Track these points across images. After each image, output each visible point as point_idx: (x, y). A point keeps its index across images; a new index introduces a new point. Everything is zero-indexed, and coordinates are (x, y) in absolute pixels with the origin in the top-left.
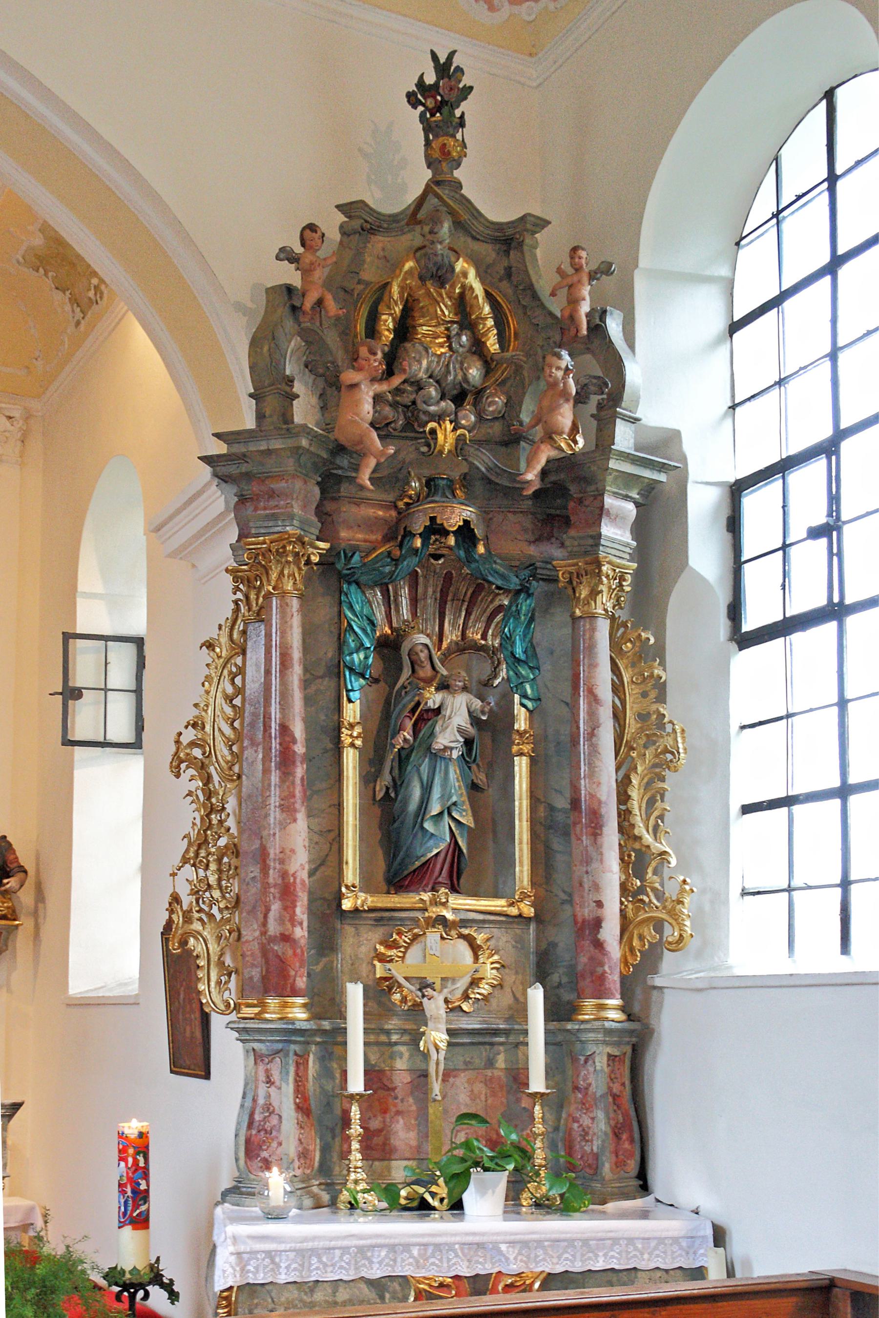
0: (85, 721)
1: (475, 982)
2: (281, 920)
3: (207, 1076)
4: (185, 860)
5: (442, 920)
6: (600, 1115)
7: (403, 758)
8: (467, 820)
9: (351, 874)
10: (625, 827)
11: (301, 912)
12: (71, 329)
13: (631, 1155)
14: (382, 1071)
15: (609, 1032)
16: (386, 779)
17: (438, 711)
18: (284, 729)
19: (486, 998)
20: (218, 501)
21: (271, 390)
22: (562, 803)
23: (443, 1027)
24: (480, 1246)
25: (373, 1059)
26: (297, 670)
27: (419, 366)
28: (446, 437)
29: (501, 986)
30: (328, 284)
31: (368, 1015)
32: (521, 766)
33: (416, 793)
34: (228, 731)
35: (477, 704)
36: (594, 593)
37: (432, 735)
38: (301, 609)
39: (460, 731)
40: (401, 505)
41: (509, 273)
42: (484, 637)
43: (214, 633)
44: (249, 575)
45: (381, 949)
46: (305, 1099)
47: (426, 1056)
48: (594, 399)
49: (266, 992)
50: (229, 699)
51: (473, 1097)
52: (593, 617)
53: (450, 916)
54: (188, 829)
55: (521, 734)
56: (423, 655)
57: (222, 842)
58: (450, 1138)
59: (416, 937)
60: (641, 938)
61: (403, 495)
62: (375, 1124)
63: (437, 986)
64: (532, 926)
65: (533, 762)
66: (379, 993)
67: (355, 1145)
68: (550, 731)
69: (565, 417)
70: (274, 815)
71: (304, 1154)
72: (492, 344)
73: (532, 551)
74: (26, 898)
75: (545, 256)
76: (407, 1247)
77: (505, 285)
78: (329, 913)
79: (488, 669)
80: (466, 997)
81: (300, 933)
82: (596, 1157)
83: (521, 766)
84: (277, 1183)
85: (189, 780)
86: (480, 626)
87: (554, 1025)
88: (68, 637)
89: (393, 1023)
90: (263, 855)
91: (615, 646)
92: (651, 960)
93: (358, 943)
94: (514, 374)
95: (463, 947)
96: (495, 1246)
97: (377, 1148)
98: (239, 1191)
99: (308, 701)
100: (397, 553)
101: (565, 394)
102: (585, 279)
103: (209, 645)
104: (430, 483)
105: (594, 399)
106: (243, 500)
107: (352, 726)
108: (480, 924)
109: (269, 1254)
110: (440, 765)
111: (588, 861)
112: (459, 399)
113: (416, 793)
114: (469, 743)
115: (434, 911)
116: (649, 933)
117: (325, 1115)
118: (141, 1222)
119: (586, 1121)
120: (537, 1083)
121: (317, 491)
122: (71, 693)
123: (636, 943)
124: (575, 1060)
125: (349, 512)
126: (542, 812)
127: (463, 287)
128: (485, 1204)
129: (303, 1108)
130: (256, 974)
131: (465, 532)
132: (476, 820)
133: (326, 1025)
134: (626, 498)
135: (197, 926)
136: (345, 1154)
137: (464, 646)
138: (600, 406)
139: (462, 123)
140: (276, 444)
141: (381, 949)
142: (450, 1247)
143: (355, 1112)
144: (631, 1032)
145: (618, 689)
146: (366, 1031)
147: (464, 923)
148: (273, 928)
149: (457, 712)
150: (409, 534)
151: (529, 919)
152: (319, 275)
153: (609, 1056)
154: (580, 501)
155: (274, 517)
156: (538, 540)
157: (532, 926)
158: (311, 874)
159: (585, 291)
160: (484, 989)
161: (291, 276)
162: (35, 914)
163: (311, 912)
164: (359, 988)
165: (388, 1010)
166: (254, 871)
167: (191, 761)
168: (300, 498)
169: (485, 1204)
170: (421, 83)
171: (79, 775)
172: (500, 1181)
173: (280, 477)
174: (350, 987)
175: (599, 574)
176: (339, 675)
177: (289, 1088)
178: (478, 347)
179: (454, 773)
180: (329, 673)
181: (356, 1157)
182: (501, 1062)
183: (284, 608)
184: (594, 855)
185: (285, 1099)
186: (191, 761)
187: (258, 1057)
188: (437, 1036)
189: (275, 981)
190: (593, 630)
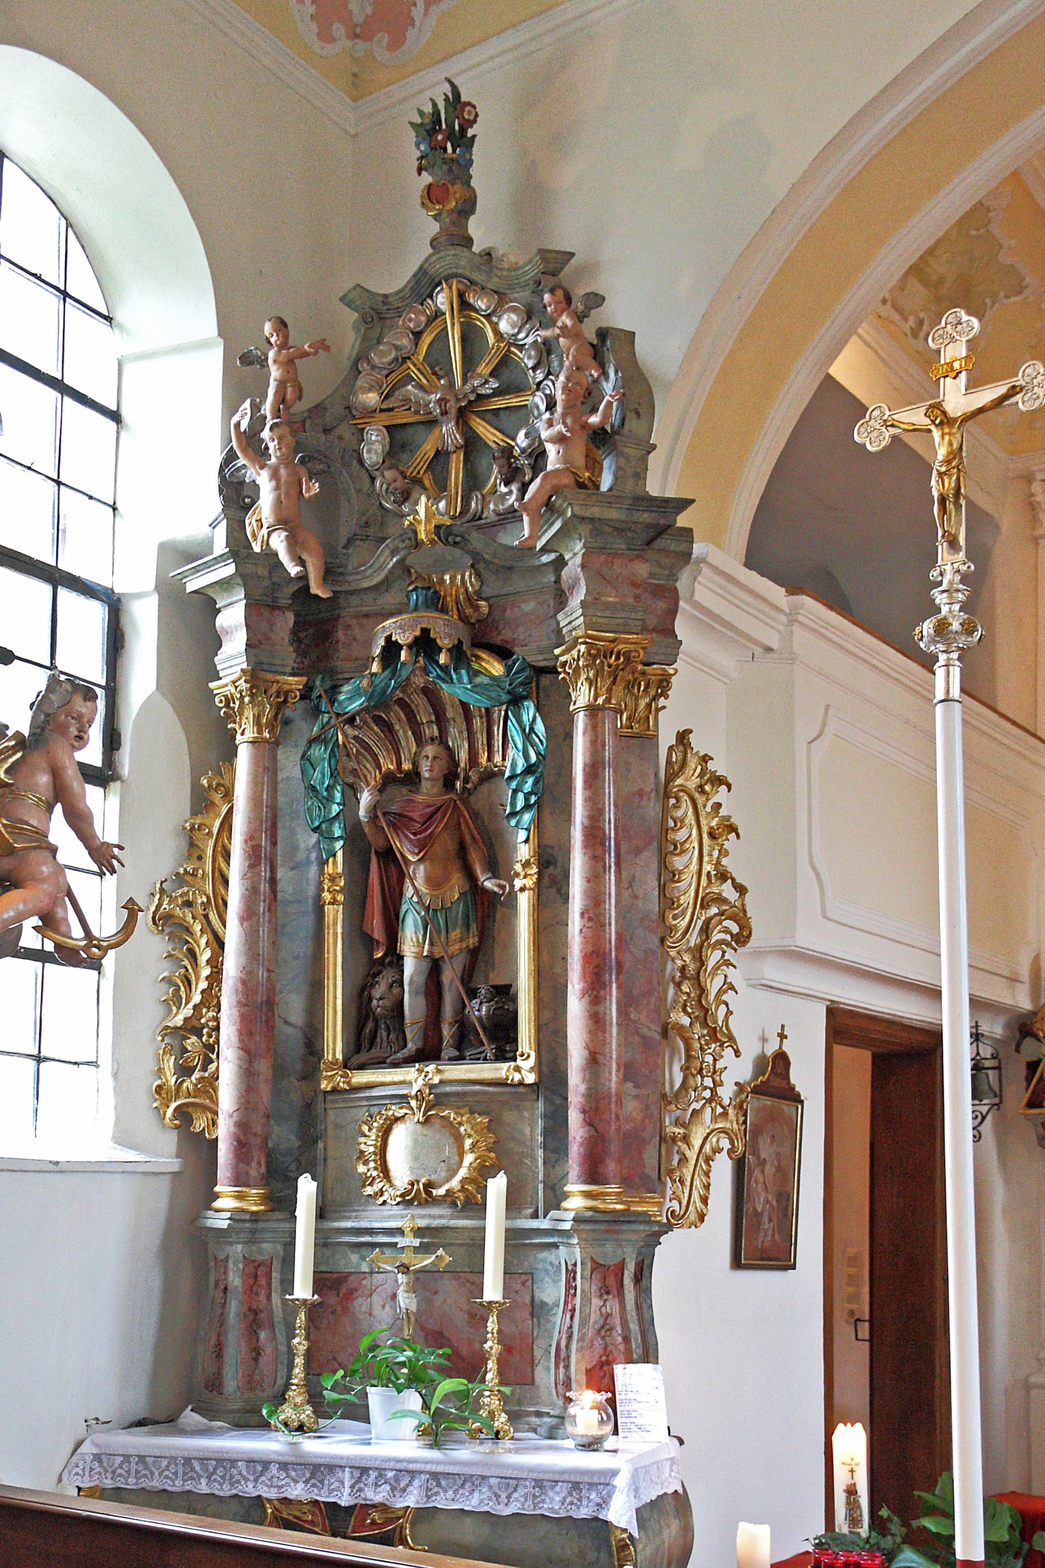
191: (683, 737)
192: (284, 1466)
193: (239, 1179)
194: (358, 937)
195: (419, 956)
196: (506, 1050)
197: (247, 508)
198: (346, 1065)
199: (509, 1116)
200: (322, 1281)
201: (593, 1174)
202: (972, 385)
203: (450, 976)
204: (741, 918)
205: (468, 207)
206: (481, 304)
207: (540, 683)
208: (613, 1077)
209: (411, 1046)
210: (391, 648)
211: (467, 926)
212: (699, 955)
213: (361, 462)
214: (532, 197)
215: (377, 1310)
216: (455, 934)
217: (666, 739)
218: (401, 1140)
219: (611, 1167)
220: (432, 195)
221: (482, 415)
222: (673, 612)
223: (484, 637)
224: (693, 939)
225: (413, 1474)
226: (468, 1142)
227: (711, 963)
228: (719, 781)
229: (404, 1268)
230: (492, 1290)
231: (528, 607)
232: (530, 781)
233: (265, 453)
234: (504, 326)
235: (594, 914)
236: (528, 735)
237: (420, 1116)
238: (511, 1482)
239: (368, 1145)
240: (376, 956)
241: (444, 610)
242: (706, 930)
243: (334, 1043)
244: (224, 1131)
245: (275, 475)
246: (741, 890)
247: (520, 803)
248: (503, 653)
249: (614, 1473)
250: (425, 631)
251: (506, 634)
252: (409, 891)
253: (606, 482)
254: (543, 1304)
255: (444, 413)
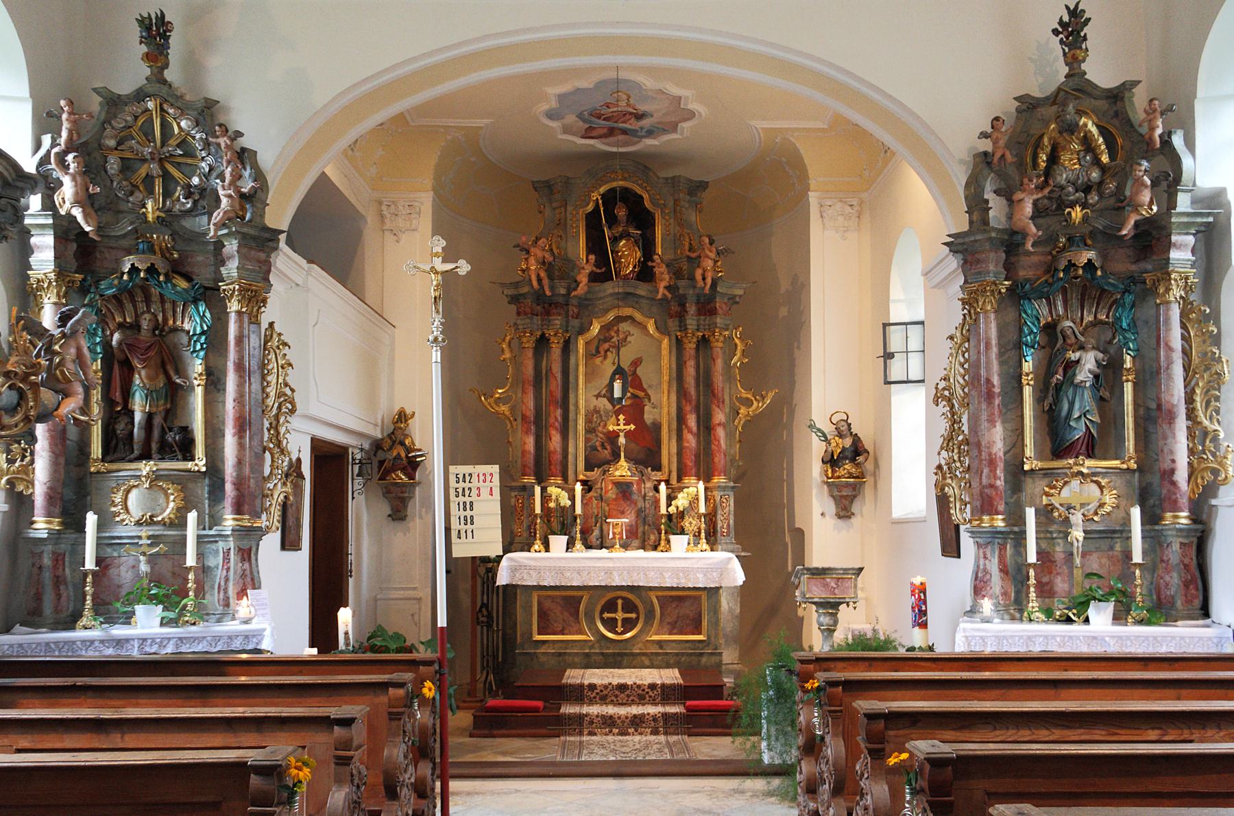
0: (897, 370)
1: (1102, 505)
2: (988, 477)
3: (959, 557)
4: (942, 448)
5: (1081, 473)
6: (1175, 575)
7: (1058, 388)
8: (1096, 419)
9: (1029, 451)
10: (1191, 415)
11: (1000, 472)
12: (883, 154)
13: (1196, 597)
14: (1048, 553)
15: (1180, 530)
16: (1050, 399)
17: (1078, 362)
18: (988, 381)
19: (1108, 514)
20: (953, 263)
21: (977, 205)
22: (1153, 406)
23: (1081, 529)
24: (1094, 638)
25: (1044, 545)
26: (995, 350)
27: (1062, 177)
28: (1077, 214)
29: (1118, 507)
30: (1007, 146)
31: (1038, 524)
32: (1128, 388)
33: (1066, 407)
34: (962, 381)
35: (1100, 355)
36: (1168, 290)
37: (1074, 375)
38: (996, 318)
39: (1090, 371)
40: (1054, 253)
41: (1116, 114)
42: (1107, 317)
43: (953, 331)
44: (969, 302)
45: (1047, 489)
46: (1005, 566)
47: (1072, 544)
48: (1164, 184)
49: (983, 513)
50: (962, 365)
51: (1101, 566)
52: (1168, 303)
53: (1085, 471)
54: (943, 432)
55: (1128, 370)
56: (1069, 332)
57: (960, 438)
58: (1080, 584)
59: (1066, 483)
60: (1203, 478)
61: (1056, 247)
62: (1045, 580)
63: (1078, 507)
64: (1137, 474)
65: (1135, 385)
66: (1045, 514)
67: (1032, 589)
68: (1147, 367)
69: (1146, 196)
70: (984, 425)
71: (1005, 594)
72: (1105, 159)
73: (1133, 267)
74: (869, 466)
75: (1139, 101)
76: (1054, 637)
77: (1115, 121)
78: (1017, 473)
79: (1110, 335)
80: (1096, 513)
81: (1000, 483)
82: (1173, 597)
83: (1128, 388)
84: (987, 605)
85: (943, 408)
86: (1105, 311)
87: (1148, 527)
88: (885, 325)
89: (1053, 528)
90: (979, 445)
91: (1184, 315)
92: (1210, 490)
93: (1035, 487)
94: (1120, 172)
95: (1094, 487)
96: (1103, 639)
97: (1045, 591)
98: (972, 612)
99: (1001, 363)
100: (1051, 280)
101: (1144, 185)
102: (1158, 115)
103: (951, 338)
104: (1070, 239)
105: (1164, 184)
106: (965, 262)
107: (1027, 375)
108: (1104, 475)
109: (981, 637)
110: (1079, 391)
111: (1165, 438)
112: (1087, 189)
113: (1066, 407)
114: (1096, 377)
115: (1076, 469)
116: (1209, 476)
117: (1016, 574)
118: (924, 625)
119: (1167, 578)
120: (1137, 558)
121: (1004, 255)
122: (888, 356)
123: (1199, 481)
124: (1161, 546)
125: (1024, 261)
126: (1142, 411)
127: (1086, 133)
128: (1101, 616)
129: (1004, 570)
130: (978, 504)
131: (1090, 265)
132: (1101, 417)
133: (1016, 529)
134: (1187, 234)
135: (949, 481)
136: (1028, 593)
137: (1096, 323)
138: (1169, 186)
139: (1085, 38)
140: (979, 237)
141: (1047, 489)
142: (1078, 638)
143: (1032, 573)
144: (1196, 530)
145: (1185, 338)
146: (1037, 532)
147: (1094, 474)
148: (985, 481)
149: (1089, 362)
150: (1056, 270)
151: (1134, 471)
152: (1002, 143)
153: (1181, 543)
154: (1159, 239)
155: (980, 273)
156: (1137, 261)
157: (1137, 474)
158: (1005, 454)
159: (1159, 122)
160: (1108, 509)
161: (986, 145)
162: (874, 474)
163: (1005, 470)
164: (1033, 510)
165: (1051, 520)
166: (975, 453)
167: (944, 398)
168: (993, 265)
169: (1101, 616)
170: (1061, 22)
171: (894, 399)
172: (1109, 608)
173: (983, 252)
174: (1027, 509)
175: (1170, 279)
176: (1020, 348)
177: (996, 561)
178: (1097, 161)
179: (1087, 395)
180: (1013, 348)
181: (1033, 595)
182: (1118, 547)
183: (986, 318)
184: (1168, 432)
185: (994, 566)
186: (944, 398)
187: (979, 545)
188: (1078, 534)
189: (986, 506)
190: (1168, 310)
191: (271, 325)
192: (102, 642)
193: (49, 514)
194: (108, 399)
195: (143, 412)
196: (188, 455)
197: (54, 190)
198: (103, 460)
199: (190, 485)
200: (99, 561)
201: (238, 509)
202: (443, 261)
203: (157, 420)
204: (292, 403)
205: (166, 66)
206: (171, 111)
207: (210, 294)
208: (247, 470)
209: (136, 452)
210: (134, 270)
211: (166, 400)
212: (277, 417)
213: (106, 171)
214: (194, 66)
215: (123, 573)
216: (162, 402)
217: (265, 325)
218: (133, 496)
219: (246, 507)
220: (147, 57)
221: (172, 163)
222: (269, 271)
223: (178, 269)
224: (274, 411)
225: (169, 639)
226: (172, 497)
227: (281, 421)
228: (285, 344)
229: (144, 554)
230: (191, 561)
231: (200, 258)
232: (203, 338)
233: (67, 167)
234: (183, 124)
235: (240, 399)
236: (202, 317)
237: (147, 485)
238: (217, 638)
239: (118, 498)
240: (116, 412)
241: (155, 254)
242: (279, 408)
243: (96, 449)
244: (39, 492)
245: (74, 179)
246: (293, 390)
247: (198, 347)
248: (188, 278)
249: (264, 630)
250: (153, 265)
251: (188, 269)
252: (137, 382)
253: (248, 216)
254: (209, 567)
255: (153, 159)
